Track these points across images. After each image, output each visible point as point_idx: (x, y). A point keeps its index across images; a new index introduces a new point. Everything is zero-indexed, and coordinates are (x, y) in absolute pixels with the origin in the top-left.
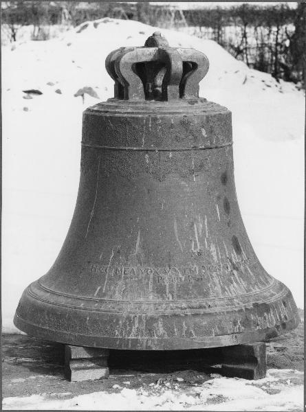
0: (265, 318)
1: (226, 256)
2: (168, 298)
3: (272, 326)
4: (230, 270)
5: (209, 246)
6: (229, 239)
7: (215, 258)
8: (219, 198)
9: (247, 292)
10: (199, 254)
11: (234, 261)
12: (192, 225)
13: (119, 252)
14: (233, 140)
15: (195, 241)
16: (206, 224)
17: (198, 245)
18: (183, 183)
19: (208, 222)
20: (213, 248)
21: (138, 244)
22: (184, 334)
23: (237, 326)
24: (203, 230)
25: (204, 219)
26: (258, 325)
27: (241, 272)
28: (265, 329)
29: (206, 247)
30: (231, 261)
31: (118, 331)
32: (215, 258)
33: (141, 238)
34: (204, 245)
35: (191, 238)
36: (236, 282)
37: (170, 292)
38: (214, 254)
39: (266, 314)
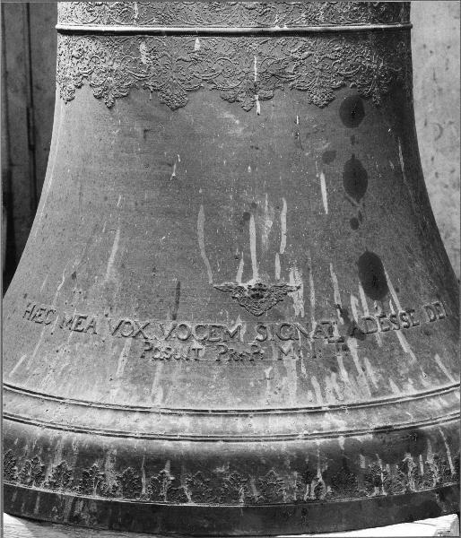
0: (404, 468)
1: (331, 302)
2: (154, 398)
3: (423, 489)
4: (336, 334)
5: (285, 274)
6: (350, 261)
7: (299, 307)
8: (328, 157)
9: (374, 394)
10: (258, 293)
11: (355, 315)
12: (247, 217)
13: (74, 276)
14: (413, 19)
15: (248, 261)
16: (284, 220)
17: (255, 269)
18: (227, 115)
19: (292, 218)
20: (295, 280)
21: (111, 260)
22: (163, 493)
23: (314, 485)
24: (276, 227)
25: (279, 207)
26: (378, 483)
27: (374, 344)
28: (399, 497)
29: (278, 276)
30: (345, 313)
31: (20, 467)
32: (299, 307)
33: (122, 237)
34: (272, 271)
35: (237, 253)
36: (350, 367)
37: (162, 382)
38: (298, 297)
39: (409, 457)
